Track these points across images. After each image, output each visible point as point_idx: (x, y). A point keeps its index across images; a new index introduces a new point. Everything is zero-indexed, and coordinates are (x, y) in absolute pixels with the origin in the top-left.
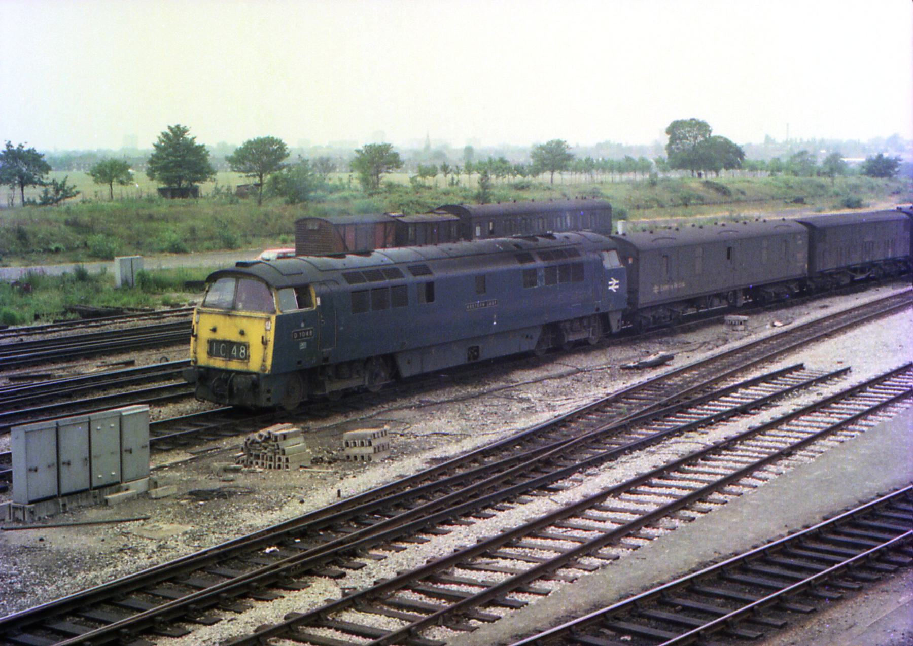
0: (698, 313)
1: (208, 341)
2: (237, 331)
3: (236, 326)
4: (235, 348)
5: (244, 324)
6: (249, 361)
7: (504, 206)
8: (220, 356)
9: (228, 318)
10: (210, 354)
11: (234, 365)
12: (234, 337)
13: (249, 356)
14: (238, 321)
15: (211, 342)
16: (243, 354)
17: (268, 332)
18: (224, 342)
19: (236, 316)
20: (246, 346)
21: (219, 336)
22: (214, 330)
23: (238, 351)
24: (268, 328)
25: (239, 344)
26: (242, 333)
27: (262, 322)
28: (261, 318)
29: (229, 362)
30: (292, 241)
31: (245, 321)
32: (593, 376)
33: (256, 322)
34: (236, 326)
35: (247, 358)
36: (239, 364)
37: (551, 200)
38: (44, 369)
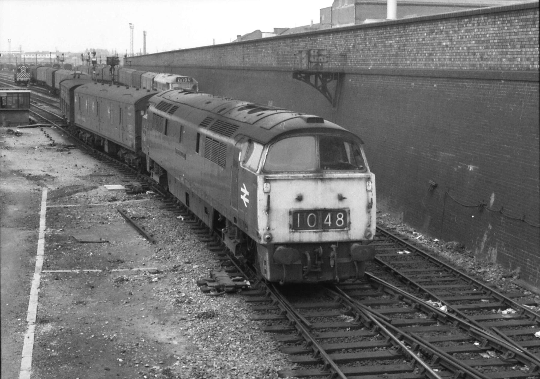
0: (240, 162)
1: (290, 213)
2: (334, 196)
3: (332, 191)
4: (329, 216)
5: (340, 187)
6: (349, 229)
7: (327, 71)
8: (307, 228)
9: (320, 183)
10: (294, 227)
11: (331, 236)
12: (331, 203)
13: (350, 223)
14: (333, 185)
15: (294, 214)
16: (340, 222)
17: (370, 193)
18: (315, 211)
19: (331, 179)
20: (345, 212)
21: (305, 205)
22: (300, 199)
23: (333, 219)
24: (369, 188)
25: (334, 212)
26: (341, 198)
27: (362, 183)
28: (360, 179)
29: (324, 233)
30: (83, 64)
31: (342, 184)
32: (78, 210)
33: (355, 183)
34: (332, 191)
35: (347, 225)
36: (335, 233)
37: (94, 53)
38: (284, 300)
